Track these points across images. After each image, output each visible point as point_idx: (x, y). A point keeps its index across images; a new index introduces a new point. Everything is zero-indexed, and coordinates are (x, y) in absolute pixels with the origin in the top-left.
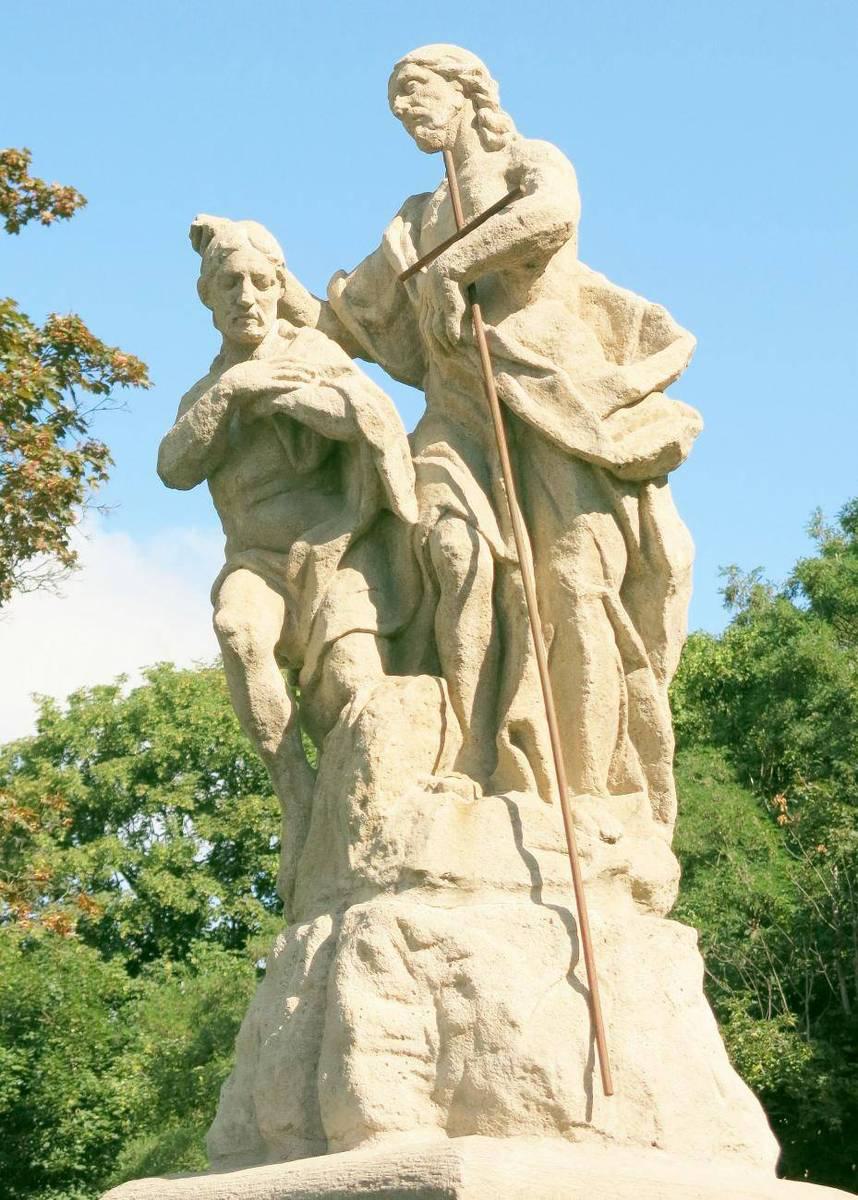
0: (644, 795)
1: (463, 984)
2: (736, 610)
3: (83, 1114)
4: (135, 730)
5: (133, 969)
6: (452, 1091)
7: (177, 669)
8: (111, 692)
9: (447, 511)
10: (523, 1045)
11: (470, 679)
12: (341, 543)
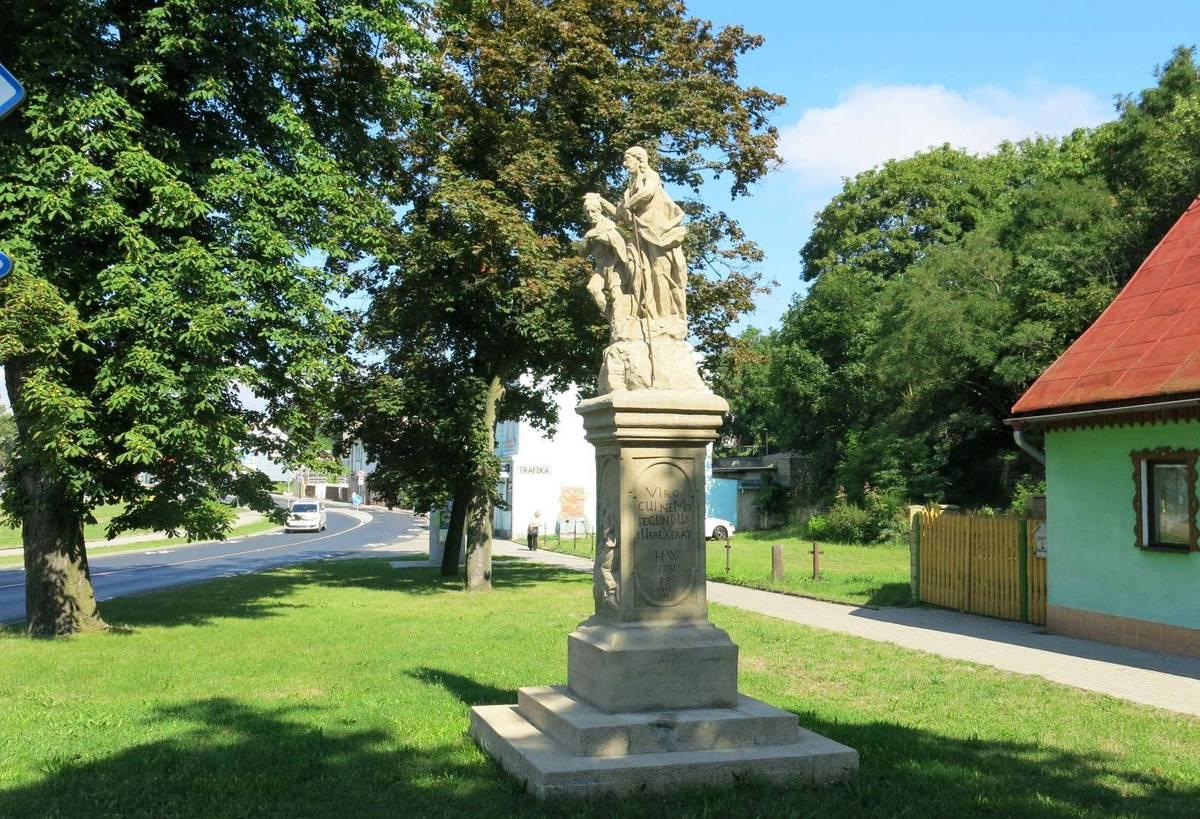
0: (678, 315)
1: (628, 360)
2: (1121, 112)
3: (859, 335)
4: (881, 187)
5: (886, 277)
6: (361, 423)
7: (897, 161)
8: (872, 172)
9: (630, 260)
10: (637, 372)
11: (638, 294)
12: (612, 267)
